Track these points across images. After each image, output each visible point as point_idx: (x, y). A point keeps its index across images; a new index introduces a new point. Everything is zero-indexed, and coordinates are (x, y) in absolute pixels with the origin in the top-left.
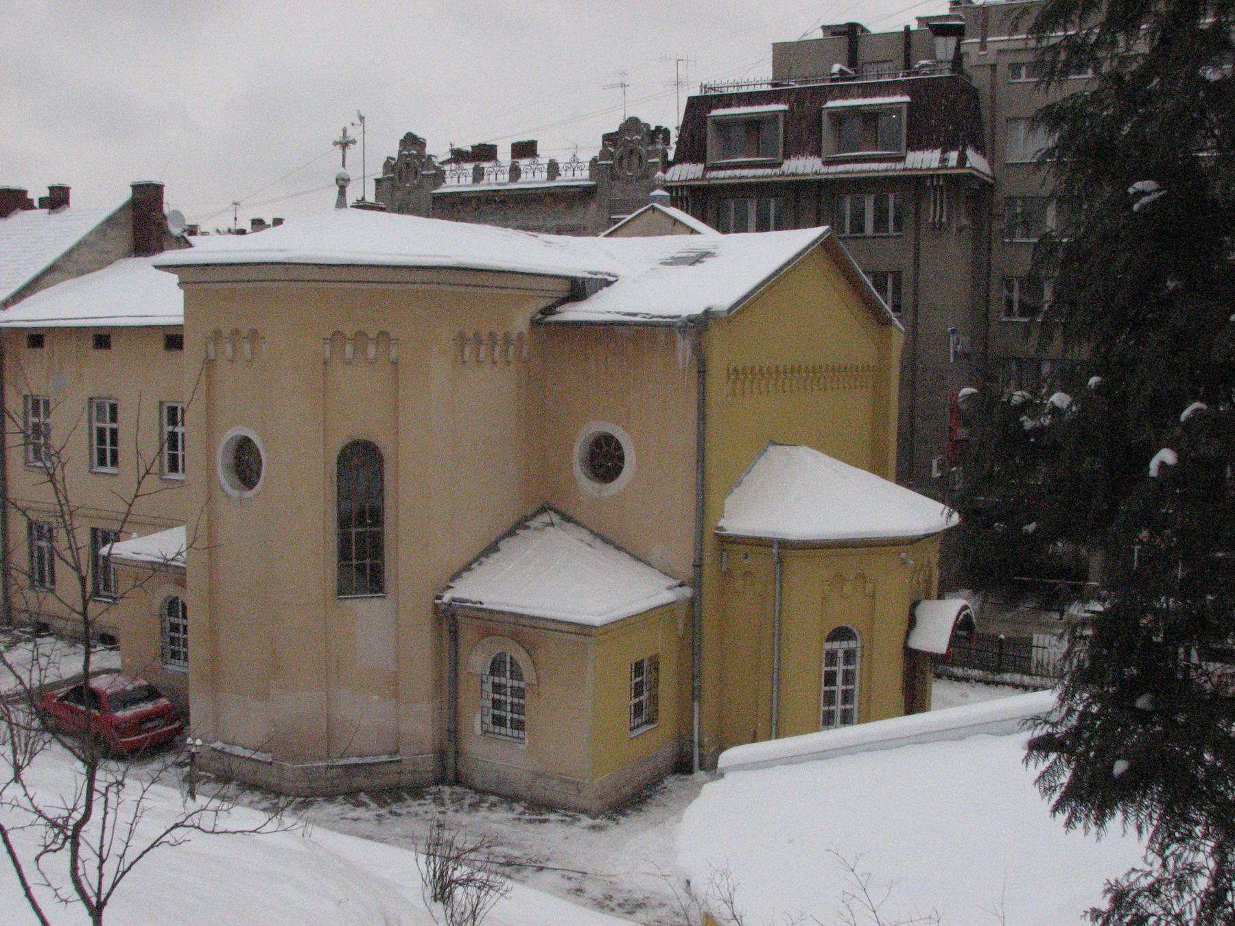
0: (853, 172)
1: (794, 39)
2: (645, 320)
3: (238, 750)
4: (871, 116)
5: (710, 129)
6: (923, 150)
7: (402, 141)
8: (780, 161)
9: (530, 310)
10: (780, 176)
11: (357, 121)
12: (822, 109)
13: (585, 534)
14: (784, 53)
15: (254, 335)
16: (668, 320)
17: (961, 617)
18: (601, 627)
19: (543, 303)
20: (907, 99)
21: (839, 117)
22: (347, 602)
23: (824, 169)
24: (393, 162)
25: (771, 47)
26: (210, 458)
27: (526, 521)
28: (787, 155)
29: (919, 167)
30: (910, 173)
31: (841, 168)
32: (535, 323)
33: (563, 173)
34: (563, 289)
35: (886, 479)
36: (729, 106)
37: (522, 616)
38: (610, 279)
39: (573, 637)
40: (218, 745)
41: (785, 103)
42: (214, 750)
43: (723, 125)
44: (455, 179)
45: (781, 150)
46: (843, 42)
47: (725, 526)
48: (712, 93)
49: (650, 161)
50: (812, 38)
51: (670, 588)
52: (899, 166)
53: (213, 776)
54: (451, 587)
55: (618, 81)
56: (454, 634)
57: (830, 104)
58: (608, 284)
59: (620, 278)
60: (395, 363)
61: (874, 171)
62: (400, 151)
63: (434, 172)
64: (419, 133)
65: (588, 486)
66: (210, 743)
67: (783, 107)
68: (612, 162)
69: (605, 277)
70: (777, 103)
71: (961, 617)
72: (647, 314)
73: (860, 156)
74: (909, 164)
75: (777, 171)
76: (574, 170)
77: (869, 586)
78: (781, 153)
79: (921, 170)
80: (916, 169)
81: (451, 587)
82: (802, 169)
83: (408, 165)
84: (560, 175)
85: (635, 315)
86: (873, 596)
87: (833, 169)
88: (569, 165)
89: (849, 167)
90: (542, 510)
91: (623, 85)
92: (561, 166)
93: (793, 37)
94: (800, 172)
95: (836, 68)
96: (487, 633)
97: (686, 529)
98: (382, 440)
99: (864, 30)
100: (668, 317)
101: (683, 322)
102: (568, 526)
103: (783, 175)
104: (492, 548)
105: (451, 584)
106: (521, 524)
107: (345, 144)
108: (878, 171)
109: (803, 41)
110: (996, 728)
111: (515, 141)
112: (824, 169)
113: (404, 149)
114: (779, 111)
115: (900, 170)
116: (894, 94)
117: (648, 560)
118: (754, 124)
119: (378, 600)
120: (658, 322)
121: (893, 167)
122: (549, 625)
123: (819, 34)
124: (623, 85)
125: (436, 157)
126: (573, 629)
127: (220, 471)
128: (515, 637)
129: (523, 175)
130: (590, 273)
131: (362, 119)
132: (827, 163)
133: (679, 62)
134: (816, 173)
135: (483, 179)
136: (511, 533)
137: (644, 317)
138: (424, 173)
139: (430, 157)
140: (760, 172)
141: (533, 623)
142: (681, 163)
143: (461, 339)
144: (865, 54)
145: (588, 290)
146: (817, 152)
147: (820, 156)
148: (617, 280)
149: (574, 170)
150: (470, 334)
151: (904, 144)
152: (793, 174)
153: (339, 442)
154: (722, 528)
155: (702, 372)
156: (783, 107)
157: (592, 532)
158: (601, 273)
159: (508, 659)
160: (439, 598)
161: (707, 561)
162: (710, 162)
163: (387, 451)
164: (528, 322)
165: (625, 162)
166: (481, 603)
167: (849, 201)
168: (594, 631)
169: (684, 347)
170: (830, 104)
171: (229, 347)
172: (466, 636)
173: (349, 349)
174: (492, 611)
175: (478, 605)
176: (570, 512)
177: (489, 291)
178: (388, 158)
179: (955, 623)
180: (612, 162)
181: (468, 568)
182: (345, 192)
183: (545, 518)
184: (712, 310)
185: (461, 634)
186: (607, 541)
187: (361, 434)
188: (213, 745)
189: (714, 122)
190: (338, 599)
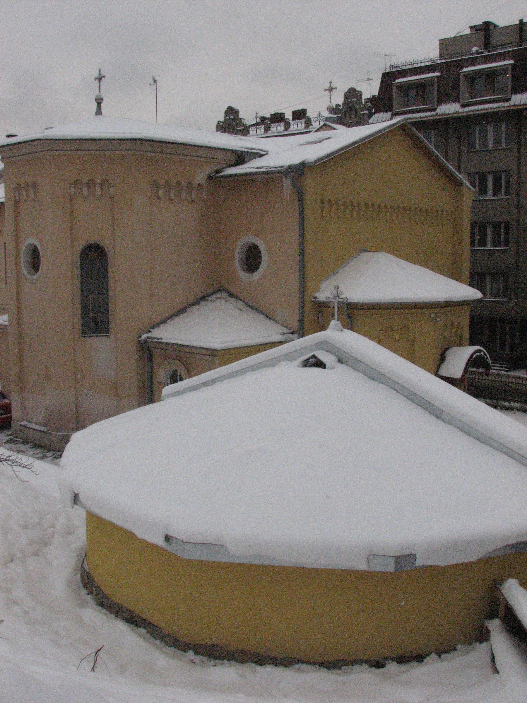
0: (478, 110)
1: (452, 35)
2: (267, 170)
3: (34, 426)
4: (490, 75)
5: (394, 90)
6: (522, 93)
7: (226, 112)
8: (436, 107)
9: (208, 169)
10: (435, 115)
11: (152, 83)
12: (459, 74)
13: (240, 304)
14: (444, 44)
15: (35, 186)
16: (275, 169)
17: (474, 356)
18: (220, 350)
19: (217, 167)
20: (512, 62)
21: (472, 78)
22: (87, 339)
23: (461, 110)
24: (221, 124)
25: (438, 42)
26: (17, 257)
27: (208, 297)
28: (439, 103)
29: (518, 104)
30: (513, 108)
31: (471, 108)
32: (210, 178)
33: (313, 123)
34: (232, 158)
35: (461, 282)
36: (405, 76)
37: (181, 345)
38: (262, 153)
39: (206, 358)
40: (24, 423)
41: (439, 72)
42: (21, 425)
43: (405, 89)
44: (255, 132)
45: (436, 100)
46: (481, 33)
47: (318, 296)
48: (396, 69)
49: (361, 113)
50: (463, 34)
51: (283, 334)
52: (507, 104)
53: (21, 441)
54: (151, 332)
55: (366, 77)
56: (151, 357)
57: (465, 70)
58: (261, 156)
59: (269, 153)
60: (113, 198)
61: (491, 108)
62: (225, 117)
63: (243, 128)
64: (235, 106)
65: (243, 276)
66: (20, 422)
67: (437, 74)
68: (340, 115)
69: (258, 151)
70: (434, 72)
71: (474, 356)
72: (269, 167)
73: (484, 100)
74: (512, 103)
75: (433, 113)
76: (319, 122)
77: (411, 336)
78: (436, 103)
79: (520, 105)
80: (517, 105)
81: (151, 332)
82: (449, 110)
83: (229, 125)
84: (312, 125)
85: (261, 168)
86: (413, 341)
87: (466, 109)
88: (316, 119)
89: (476, 107)
90: (220, 290)
91: (369, 79)
92: (312, 120)
93: (451, 34)
94: (447, 112)
95: (474, 49)
96: (166, 357)
97: (295, 299)
98: (106, 244)
99: (495, 26)
100: (278, 167)
101: (286, 169)
102: (233, 300)
103: (437, 115)
104: (183, 311)
105: (151, 330)
106: (203, 298)
107: (100, 79)
108: (493, 108)
109: (457, 37)
110: (289, 357)
111: (294, 110)
112: (461, 110)
113: (227, 116)
114: (434, 77)
115: (507, 107)
116: (504, 60)
117: (276, 319)
118: (421, 86)
119: (105, 338)
120: (274, 171)
121: (503, 105)
122: (197, 351)
123: (468, 31)
124: (369, 79)
125: (245, 119)
126: (206, 352)
127: (22, 264)
128: (179, 359)
129: (292, 127)
130: (247, 148)
131: (155, 81)
132: (463, 106)
133: (387, 57)
134: (457, 113)
135: (270, 130)
136: (196, 303)
137: (266, 169)
138: (238, 129)
139: (241, 119)
140: (423, 114)
141: (188, 350)
142: (379, 113)
143: (155, 184)
144: (494, 41)
145: (246, 160)
146: (457, 99)
147: (459, 102)
148: (267, 154)
149: (319, 122)
150: (162, 182)
151: (509, 90)
152: (443, 115)
153: (80, 246)
154: (316, 298)
155: (301, 201)
156: (437, 74)
157: (246, 304)
158: (255, 149)
159: (179, 374)
160: (140, 337)
161: (307, 318)
162: (394, 112)
163: (109, 250)
164: (206, 177)
165: (348, 115)
166: (161, 339)
167: (478, 129)
168: (218, 352)
169: (287, 183)
170: (465, 70)
171: (24, 193)
172: (157, 359)
173: (85, 190)
174: (169, 344)
175: (160, 340)
176: (232, 291)
177: (178, 157)
178: (219, 122)
179: (469, 360)
180: (340, 115)
181: (164, 322)
182: (101, 106)
183: (219, 295)
184: (306, 162)
185: (154, 358)
186: (252, 308)
187: (93, 240)
188: (21, 423)
189: (397, 86)
190: (82, 337)
